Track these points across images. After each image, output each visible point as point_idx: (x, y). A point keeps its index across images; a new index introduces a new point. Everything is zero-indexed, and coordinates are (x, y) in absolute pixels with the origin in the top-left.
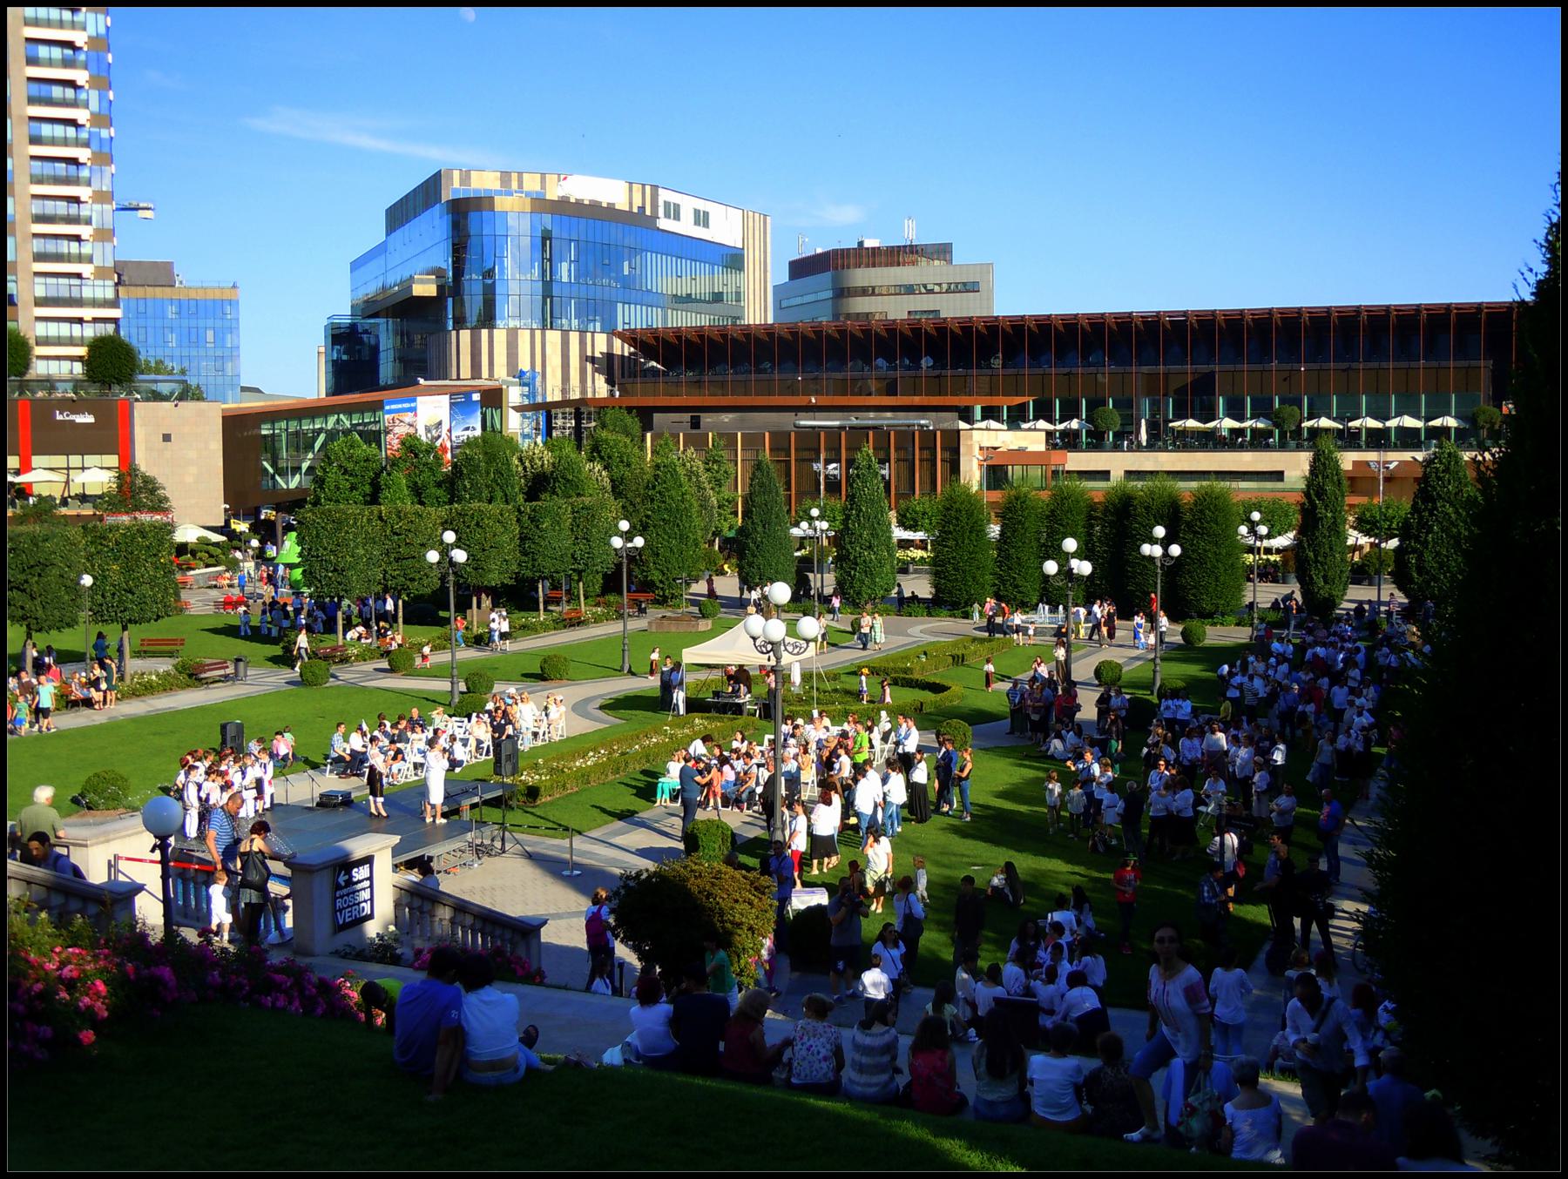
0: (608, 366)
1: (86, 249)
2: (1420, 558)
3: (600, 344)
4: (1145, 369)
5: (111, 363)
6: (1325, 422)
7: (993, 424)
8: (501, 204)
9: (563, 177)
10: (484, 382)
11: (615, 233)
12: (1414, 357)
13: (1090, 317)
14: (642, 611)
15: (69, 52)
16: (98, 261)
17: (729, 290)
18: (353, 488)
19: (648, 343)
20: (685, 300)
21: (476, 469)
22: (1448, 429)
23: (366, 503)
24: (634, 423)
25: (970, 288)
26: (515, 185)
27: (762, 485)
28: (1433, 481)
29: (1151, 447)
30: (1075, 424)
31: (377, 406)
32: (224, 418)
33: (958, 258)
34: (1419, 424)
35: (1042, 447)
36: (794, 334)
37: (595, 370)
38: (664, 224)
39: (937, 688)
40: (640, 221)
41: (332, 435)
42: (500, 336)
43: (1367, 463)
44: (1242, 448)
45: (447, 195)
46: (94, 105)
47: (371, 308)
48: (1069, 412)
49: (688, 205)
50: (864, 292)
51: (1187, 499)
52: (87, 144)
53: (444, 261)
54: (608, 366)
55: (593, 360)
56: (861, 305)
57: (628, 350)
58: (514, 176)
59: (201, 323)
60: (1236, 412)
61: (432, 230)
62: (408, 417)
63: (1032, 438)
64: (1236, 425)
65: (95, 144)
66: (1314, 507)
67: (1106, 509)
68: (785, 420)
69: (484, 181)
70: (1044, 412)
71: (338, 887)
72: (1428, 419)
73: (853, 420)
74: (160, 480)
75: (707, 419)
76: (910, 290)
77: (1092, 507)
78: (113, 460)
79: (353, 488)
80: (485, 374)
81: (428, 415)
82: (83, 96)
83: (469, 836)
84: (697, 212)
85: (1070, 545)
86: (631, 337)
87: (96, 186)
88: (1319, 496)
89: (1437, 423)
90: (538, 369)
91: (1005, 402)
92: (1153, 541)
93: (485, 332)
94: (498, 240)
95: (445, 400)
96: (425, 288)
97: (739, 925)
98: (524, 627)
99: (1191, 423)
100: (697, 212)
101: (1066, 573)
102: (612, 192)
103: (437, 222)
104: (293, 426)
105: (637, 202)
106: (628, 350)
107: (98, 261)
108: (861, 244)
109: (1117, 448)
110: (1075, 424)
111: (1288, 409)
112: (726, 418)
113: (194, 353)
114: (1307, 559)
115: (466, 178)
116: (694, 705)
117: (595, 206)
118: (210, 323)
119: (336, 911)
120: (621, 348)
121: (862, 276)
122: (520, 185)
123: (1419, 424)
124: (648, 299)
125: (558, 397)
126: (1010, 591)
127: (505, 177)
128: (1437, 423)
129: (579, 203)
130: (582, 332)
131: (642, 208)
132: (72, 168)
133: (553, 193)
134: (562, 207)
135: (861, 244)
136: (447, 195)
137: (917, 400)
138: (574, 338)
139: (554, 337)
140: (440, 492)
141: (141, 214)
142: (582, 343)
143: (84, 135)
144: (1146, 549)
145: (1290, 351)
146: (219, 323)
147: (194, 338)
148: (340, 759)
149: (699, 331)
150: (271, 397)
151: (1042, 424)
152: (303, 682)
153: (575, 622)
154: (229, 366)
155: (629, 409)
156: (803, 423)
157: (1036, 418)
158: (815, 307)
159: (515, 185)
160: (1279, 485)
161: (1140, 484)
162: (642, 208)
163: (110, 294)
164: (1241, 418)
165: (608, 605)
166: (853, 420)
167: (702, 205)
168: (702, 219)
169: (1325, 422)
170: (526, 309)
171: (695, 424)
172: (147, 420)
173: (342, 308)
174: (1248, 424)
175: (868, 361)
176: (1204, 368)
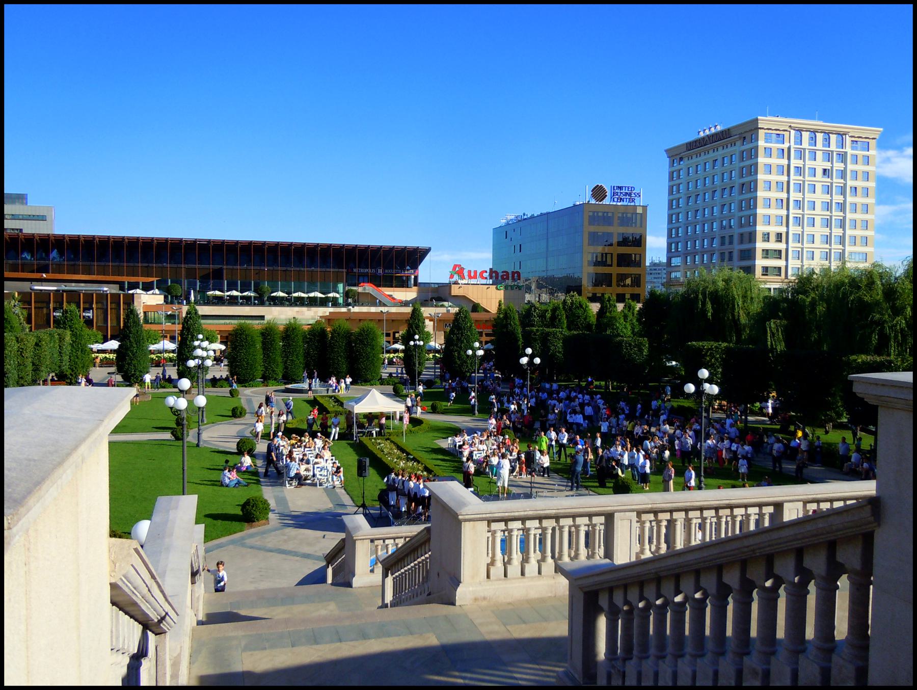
2: (459, 353)
6: (235, 293)
12: (121, 261)
22: (250, 297)
25: (43, 218)
33: (31, 202)
73: (63, 287)
89: (245, 294)
156: (36, 288)
166: (63, 287)
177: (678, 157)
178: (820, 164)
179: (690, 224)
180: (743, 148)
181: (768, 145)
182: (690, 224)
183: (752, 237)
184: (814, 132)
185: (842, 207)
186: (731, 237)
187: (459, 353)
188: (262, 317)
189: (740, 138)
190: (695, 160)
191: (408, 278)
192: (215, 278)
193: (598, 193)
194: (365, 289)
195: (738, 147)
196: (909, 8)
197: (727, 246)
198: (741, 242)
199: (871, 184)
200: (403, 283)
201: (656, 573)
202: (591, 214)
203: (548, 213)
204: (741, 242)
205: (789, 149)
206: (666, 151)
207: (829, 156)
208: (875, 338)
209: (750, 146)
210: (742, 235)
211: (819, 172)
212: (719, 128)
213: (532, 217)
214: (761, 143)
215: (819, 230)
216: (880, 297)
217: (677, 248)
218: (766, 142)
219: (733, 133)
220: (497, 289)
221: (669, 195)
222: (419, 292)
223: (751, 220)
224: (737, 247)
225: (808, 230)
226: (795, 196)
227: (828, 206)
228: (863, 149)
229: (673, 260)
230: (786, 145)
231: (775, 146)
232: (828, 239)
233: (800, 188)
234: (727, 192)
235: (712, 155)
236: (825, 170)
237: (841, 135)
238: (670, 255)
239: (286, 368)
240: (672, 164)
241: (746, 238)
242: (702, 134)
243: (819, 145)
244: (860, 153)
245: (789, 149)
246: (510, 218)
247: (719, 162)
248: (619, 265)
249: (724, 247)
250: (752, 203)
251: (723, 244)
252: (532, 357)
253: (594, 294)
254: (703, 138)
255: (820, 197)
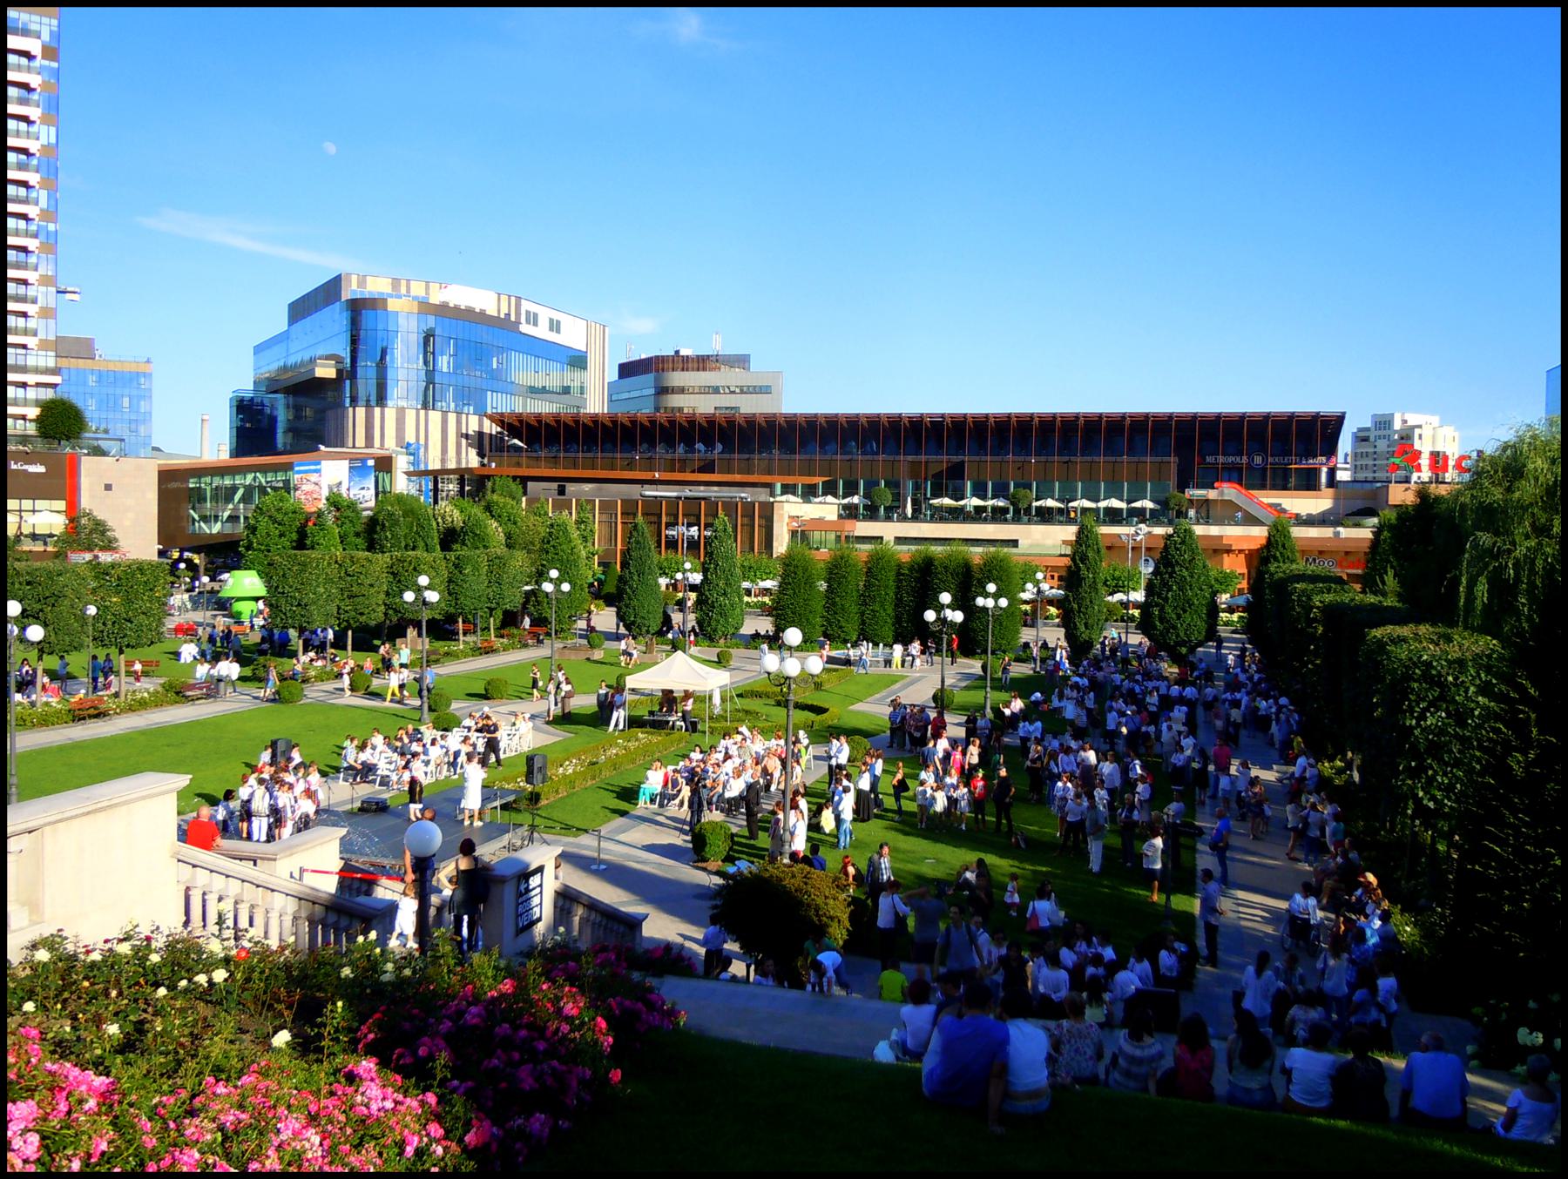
0: (480, 442)
1: (32, 324)
2: (1162, 610)
3: (473, 424)
4: (910, 458)
5: (61, 421)
7: (791, 497)
8: (393, 304)
9: (443, 285)
10: (376, 451)
11: (484, 334)
13: (868, 416)
14: (540, 642)
15: (23, 157)
16: (41, 335)
17: (576, 384)
18: (281, 535)
19: (515, 426)
20: (534, 391)
21: (396, 523)
23: (294, 548)
24: (516, 487)
26: (403, 290)
27: (638, 542)
28: (1172, 551)
29: (916, 518)
30: (855, 500)
31: (288, 467)
32: (160, 473)
33: (753, 366)
34: (1123, 505)
35: (835, 517)
36: (634, 422)
37: (469, 445)
38: (525, 328)
39: (819, 710)
40: (505, 325)
41: (249, 490)
42: (390, 413)
43: (1119, 536)
44: (985, 521)
45: (346, 295)
46: (43, 203)
47: (273, 385)
48: (851, 490)
49: (544, 315)
50: (682, 390)
51: (977, 561)
52: (36, 236)
53: (346, 354)
54: (480, 442)
55: (467, 436)
56: (675, 401)
57: (495, 429)
58: (403, 283)
59: (119, 391)
60: (980, 492)
61: (334, 321)
62: (314, 477)
63: (826, 509)
64: (980, 503)
65: (42, 236)
66: (1079, 569)
67: (911, 569)
68: (634, 491)
69: (377, 286)
70: (830, 489)
71: (521, 895)
72: (1129, 502)
73: (687, 492)
74: (110, 523)
75: (571, 488)
76: (716, 390)
77: (900, 566)
78: (61, 505)
79: (281, 535)
80: (377, 443)
81: (325, 478)
82: (34, 194)
83: (507, 837)
84: (551, 320)
85: (946, 598)
86: (499, 420)
87: (42, 271)
88: (1082, 560)
89: (1138, 504)
90: (422, 442)
91: (801, 481)
92: (986, 595)
93: (377, 410)
94: (391, 334)
95: (345, 464)
96: (326, 371)
97: (832, 918)
98: (447, 654)
99: (947, 501)
100: (551, 320)
101: (942, 621)
102: (484, 301)
103: (337, 316)
104: (217, 481)
105: (504, 310)
106: (495, 429)
107: (41, 335)
108: (677, 352)
109: (888, 519)
110: (855, 500)
111: (1022, 492)
112: (587, 487)
113: (111, 416)
114: (1072, 610)
115: (362, 282)
116: (634, 722)
117: (470, 311)
118: (126, 391)
119: (518, 916)
120: (490, 428)
121: (677, 378)
122: (408, 290)
123: (1123, 505)
124: (510, 389)
125: (438, 466)
126: (835, 631)
127: (396, 283)
128: (1138, 504)
129: (456, 308)
130: (459, 413)
131: (508, 315)
132: (23, 255)
133: (436, 298)
134: (443, 310)
135: (677, 352)
136: (346, 295)
137: (738, 478)
138: (452, 417)
139: (435, 417)
140: (359, 541)
141: (68, 296)
142: (459, 422)
143: (33, 227)
144: (980, 601)
145: (1023, 445)
146: (134, 392)
147: (111, 404)
148: (351, 768)
149: (557, 418)
150: (171, 456)
151: (830, 498)
152: (277, 698)
153: (489, 651)
154: (142, 429)
155: (515, 478)
157: (824, 494)
158: (639, 401)
159: (403, 290)
160: (1014, 550)
161: (940, 548)
162: (508, 315)
163: (51, 363)
164: (984, 498)
165: (510, 636)
166: (687, 492)
167: (556, 316)
168: (555, 326)
169: (1050, 503)
170: (413, 394)
171: (562, 491)
172: (91, 471)
173: (245, 384)
174: (990, 503)
175: (652, 445)
176: (955, 459)
187: (1162, 610)
188: (1015, 543)
191: (1315, 472)
192: (949, 481)
194: (1222, 493)
196: (1554, 14)
200: (1308, 483)
201: (312, 923)
216: (322, 504)
222: (1336, 499)
239: (863, 623)
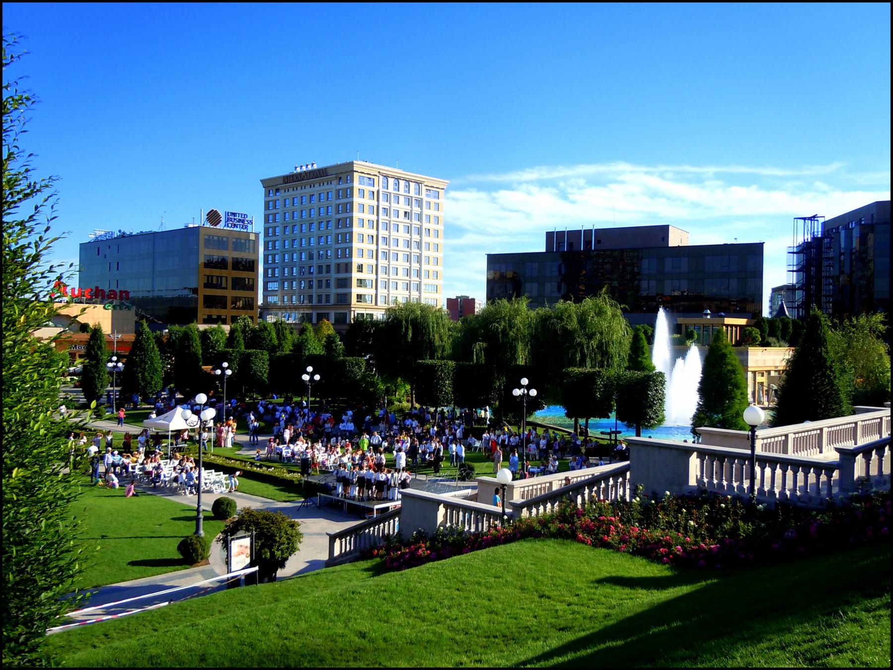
2: (143, 374)
177: (274, 189)
178: (403, 207)
179: (287, 252)
180: (339, 187)
181: (362, 187)
182: (287, 252)
183: (348, 267)
184: (398, 179)
185: (419, 245)
186: (328, 266)
189: (336, 178)
190: (291, 192)
193: (213, 217)
195: (334, 186)
197: (324, 274)
198: (338, 271)
199: (440, 227)
202: (206, 237)
203: (152, 236)
204: (338, 271)
205: (378, 192)
206: (263, 182)
207: (409, 201)
208: (578, 356)
209: (343, 186)
210: (338, 265)
211: (402, 214)
212: (315, 167)
213: (131, 236)
214: (356, 185)
215: (402, 264)
217: (273, 273)
218: (360, 184)
219: (329, 172)
220: (104, 308)
221: (265, 223)
223: (347, 252)
224: (334, 276)
225: (393, 263)
226: (383, 233)
227: (408, 244)
228: (435, 197)
229: (270, 285)
230: (375, 189)
231: (367, 189)
232: (408, 272)
233: (387, 227)
234: (323, 225)
235: (308, 190)
236: (406, 213)
237: (418, 184)
238: (267, 280)
240: (268, 194)
241: (343, 267)
242: (299, 170)
243: (402, 191)
244: (433, 201)
245: (378, 192)
246: (98, 233)
247: (316, 197)
248: (233, 288)
249: (320, 275)
250: (347, 238)
251: (320, 272)
252: (312, 375)
253: (210, 316)
254: (300, 174)
255: (402, 235)
